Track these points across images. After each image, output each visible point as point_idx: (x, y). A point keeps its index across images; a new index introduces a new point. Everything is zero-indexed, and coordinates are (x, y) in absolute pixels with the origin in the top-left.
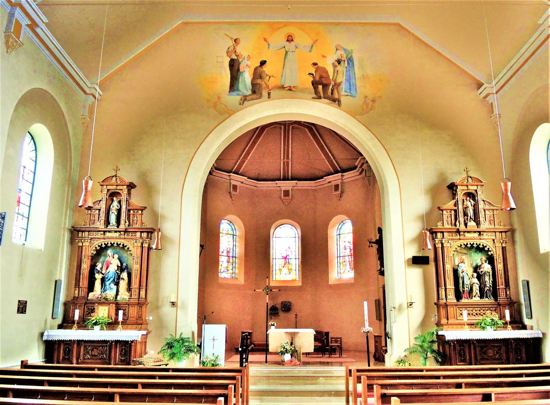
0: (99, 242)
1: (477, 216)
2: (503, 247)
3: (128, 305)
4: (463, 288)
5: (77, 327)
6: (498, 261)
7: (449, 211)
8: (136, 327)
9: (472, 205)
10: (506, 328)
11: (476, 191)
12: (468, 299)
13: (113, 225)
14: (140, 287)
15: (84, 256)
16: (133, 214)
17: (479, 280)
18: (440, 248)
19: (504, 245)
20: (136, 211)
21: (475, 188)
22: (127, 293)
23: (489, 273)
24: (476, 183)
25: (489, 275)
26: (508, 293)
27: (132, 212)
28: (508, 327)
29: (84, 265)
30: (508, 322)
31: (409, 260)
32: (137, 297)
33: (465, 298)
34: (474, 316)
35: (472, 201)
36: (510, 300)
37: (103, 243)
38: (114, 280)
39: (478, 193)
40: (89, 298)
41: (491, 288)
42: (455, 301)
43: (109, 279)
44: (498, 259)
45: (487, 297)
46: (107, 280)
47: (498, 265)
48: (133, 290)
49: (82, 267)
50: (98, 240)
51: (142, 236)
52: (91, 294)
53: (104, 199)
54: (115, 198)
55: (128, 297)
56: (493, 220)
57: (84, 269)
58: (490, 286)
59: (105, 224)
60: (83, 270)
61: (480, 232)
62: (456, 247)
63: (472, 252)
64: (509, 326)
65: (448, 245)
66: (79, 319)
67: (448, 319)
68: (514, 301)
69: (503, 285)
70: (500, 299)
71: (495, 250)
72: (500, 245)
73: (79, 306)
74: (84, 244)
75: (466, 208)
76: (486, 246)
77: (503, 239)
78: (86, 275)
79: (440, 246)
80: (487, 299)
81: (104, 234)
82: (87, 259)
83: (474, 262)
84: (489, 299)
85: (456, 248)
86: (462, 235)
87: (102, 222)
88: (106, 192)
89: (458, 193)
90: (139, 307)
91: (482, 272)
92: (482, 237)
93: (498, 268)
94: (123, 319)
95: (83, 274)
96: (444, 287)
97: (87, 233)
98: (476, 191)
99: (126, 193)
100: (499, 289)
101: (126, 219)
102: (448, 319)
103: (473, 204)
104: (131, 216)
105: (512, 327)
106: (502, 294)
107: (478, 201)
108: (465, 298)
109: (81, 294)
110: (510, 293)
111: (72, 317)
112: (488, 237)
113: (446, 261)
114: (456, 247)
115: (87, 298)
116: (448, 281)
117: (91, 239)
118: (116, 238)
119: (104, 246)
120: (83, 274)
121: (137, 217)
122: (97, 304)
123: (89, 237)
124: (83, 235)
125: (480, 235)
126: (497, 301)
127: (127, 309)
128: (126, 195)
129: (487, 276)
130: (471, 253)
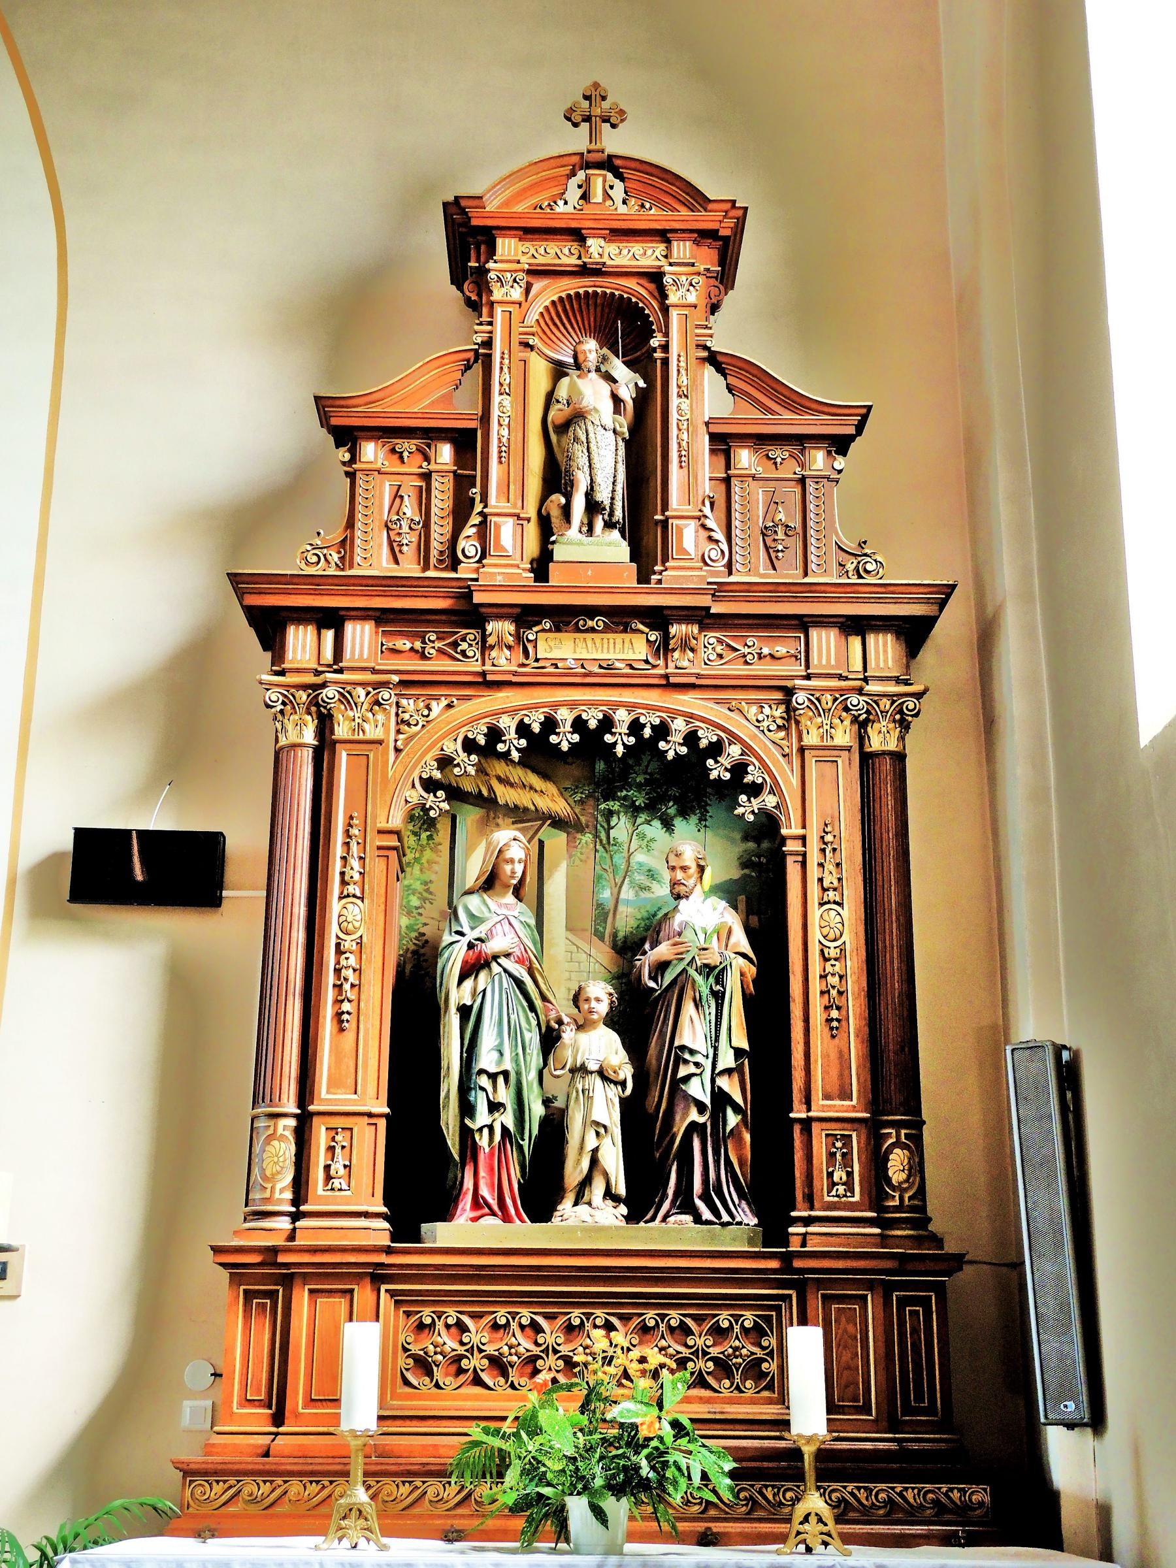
2: (867, 759)
4: (467, 1109)
6: (813, 872)
7: (407, 446)
9: (617, 400)
10: (779, 1513)
11: (655, 277)
12: (507, 1218)
17: (635, 1047)
18: (307, 755)
19: (881, 738)
21: (648, 255)
23: (719, 980)
24: (655, 216)
25: (719, 997)
26: (897, 1165)
28: (801, 1510)
30: (808, 1451)
31: (42, 870)
33: (478, 1203)
34: (477, 1381)
35: (619, 369)
36: (917, 1241)
39: (673, 298)
41: (733, 1120)
42: (379, 1232)
44: (814, 857)
45: (685, 1205)
47: (815, 913)
56: (796, 523)
57: (349, 943)
58: (720, 1099)
60: (339, 951)
61: (658, 618)
62: (453, 747)
63: (615, 805)
64: (814, 1502)
65: (372, 732)
67: (278, 1419)
68: (950, 1247)
69: (845, 1095)
70: (807, 1222)
71: (795, 781)
72: (844, 736)
75: (564, 428)
76: (716, 749)
77: (872, 687)
79: (309, 736)
80: (688, 1218)
83: (627, 893)
84: (698, 1219)
85: (445, 762)
86: (500, 643)
89: (498, 294)
91: (661, 967)
92: (682, 663)
93: (815, 935)
96: (290, 1106)
98: (655, 277)
100: (807, 1124)
102: (278, 1419)
103: (627, 394)
106: (839, 1175)
107: (666, 362)
108: (478, 1203)
110: (917, 1167)
112: (738, 669)
113: (337, 866)
114: (453, 747)
116: (336, 1050)
117: (403, 683)
125: (663, 648)
126: (784, 1240)
129: (698, 1004)
130: (610, 814)
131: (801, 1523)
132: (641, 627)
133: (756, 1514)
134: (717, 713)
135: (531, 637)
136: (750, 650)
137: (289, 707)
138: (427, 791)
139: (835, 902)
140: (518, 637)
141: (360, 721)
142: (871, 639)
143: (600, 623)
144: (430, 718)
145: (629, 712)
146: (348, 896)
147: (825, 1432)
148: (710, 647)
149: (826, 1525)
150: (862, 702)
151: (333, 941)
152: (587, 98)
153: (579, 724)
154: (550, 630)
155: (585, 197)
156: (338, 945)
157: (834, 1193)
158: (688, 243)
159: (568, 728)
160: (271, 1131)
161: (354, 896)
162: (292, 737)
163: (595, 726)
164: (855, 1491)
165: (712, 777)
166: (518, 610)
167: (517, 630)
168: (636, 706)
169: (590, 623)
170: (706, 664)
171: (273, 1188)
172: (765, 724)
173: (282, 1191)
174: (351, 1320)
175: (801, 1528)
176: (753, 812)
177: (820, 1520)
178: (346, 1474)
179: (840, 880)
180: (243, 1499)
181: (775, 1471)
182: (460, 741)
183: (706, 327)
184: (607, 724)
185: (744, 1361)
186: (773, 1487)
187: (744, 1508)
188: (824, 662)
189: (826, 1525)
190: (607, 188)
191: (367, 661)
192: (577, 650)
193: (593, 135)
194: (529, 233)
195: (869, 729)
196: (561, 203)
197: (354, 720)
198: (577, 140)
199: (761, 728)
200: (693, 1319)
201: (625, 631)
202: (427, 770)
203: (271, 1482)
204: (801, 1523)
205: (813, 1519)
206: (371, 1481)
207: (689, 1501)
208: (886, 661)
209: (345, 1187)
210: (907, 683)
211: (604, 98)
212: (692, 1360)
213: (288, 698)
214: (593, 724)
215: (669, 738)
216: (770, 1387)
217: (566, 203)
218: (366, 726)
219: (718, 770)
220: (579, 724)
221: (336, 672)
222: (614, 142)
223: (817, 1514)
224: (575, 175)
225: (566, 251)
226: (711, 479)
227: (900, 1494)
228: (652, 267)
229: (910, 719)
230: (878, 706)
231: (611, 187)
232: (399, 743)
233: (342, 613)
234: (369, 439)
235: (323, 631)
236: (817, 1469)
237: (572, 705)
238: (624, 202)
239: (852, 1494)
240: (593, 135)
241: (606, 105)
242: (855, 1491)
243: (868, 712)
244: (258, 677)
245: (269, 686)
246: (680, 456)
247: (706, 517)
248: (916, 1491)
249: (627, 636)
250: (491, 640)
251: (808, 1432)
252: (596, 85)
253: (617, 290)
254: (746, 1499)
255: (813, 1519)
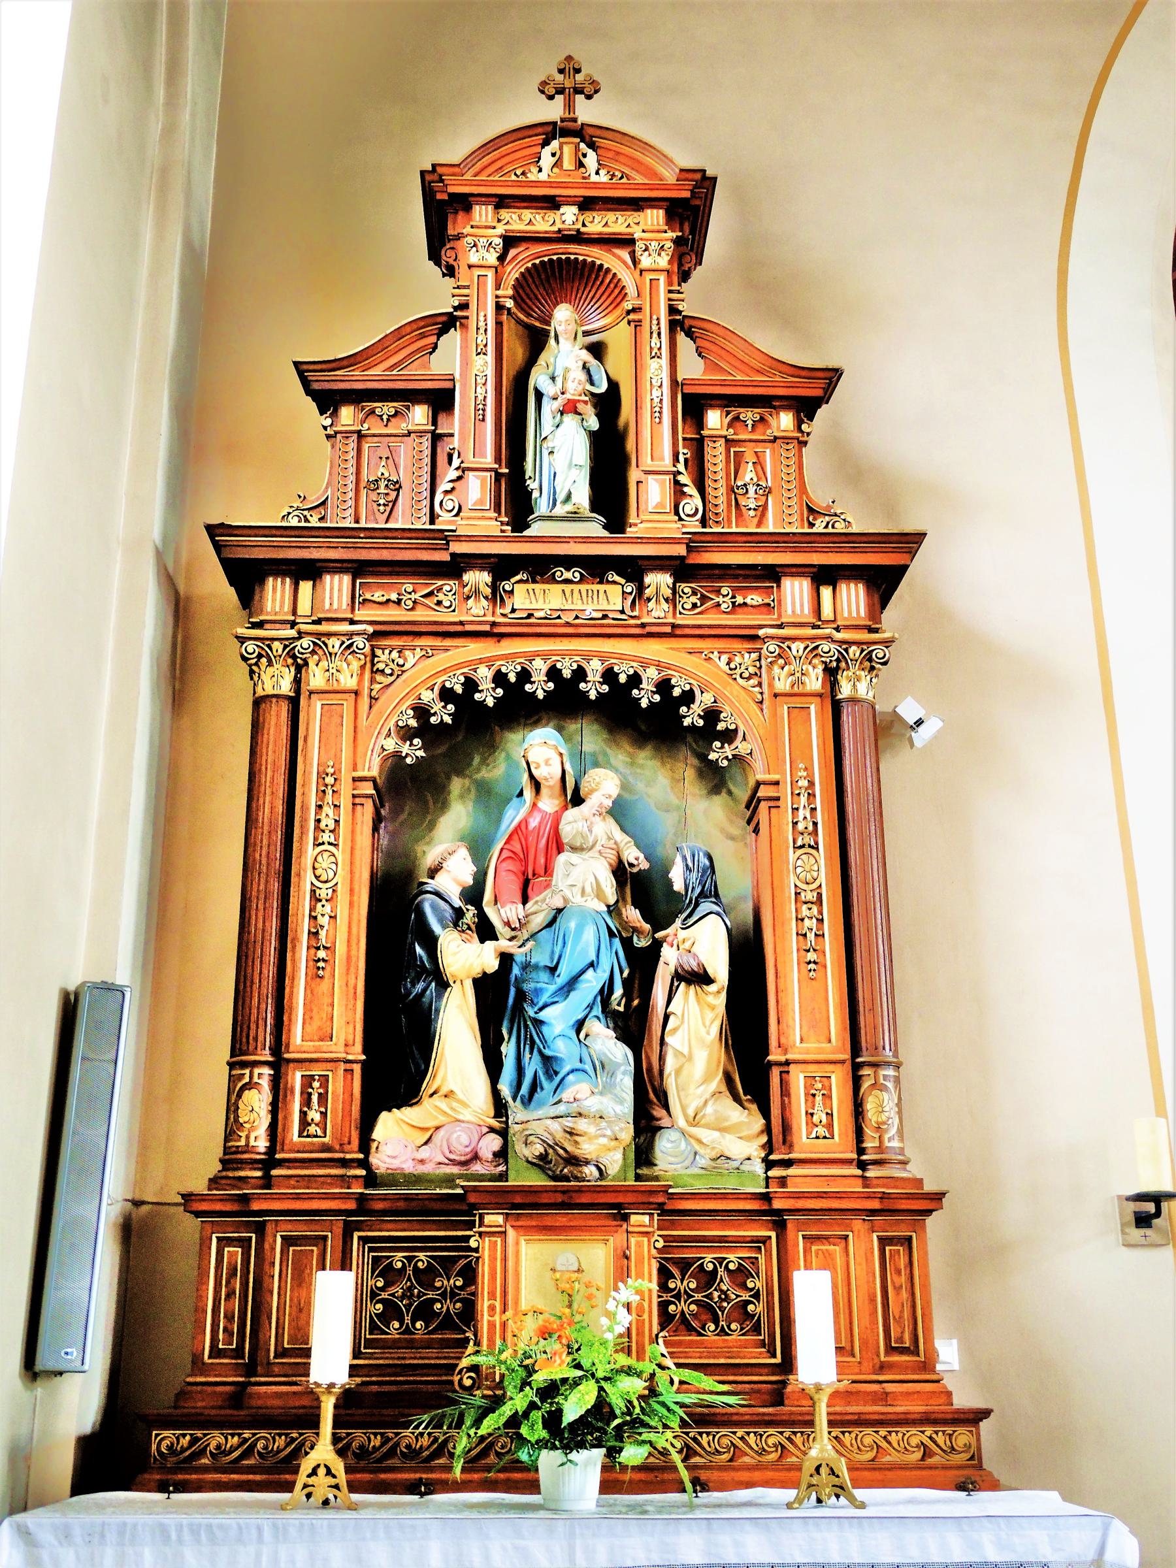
0: (441, 660)
1: (317, 1227)
3: (780, 1226)
5: (339, 1466)
8: (927, 1453)
13: (574, 517)
14: (856, 1050)
15: (322, 775)
16: (729, 442)
20: (749, 415)
22: (735, 1114)
27: (714, 419)
29: (325, 862)
32: (841, 1144)
37: (484, 675)
38: (605, 994)
40: (381, 1161)
43: (571, 985)
46: (548, 987)
48: (798, 1079)
49: (309, 877)
50: (438, 642)
51: (827, 612)
52: (388, 1125)
53: (483, 316)
54: (563, 316)
55: (754, 1149)
57: (323, 893)
59: (497, 509)
60: (315, 899)
66: (841, 1368)
73: (288, 1241)
74: (316, 678)
78: (341, 949)
81: (496, 596)
82: (345, 801)
87: (477, 489)
88: (492, 258)
90: (884, 1242)
94: (354, 1370)
95: (314, 935)
97: (337, 587)
99: (663, 261)
101: (681, 467)
104: (715, 455)
105: (541, 1388)
109: (304, 1123)
111: (215, 1352)
115: (365, 1164)
117: (377, 635)
118: (601, 627)
119: (488, 695)
120: (314, 935)
121: (759, 464)
122: (494, 1219)
123: (360, 614)
124: (304, 607)
127: (768, 1263)
128: (662, 278)
131: (309, 1476)
132: (617, 578)
133: (930, 1461)
134: (692, 663)
135: (507, 588)
136: (409, 596)
137: (264, 660)
138: (404, 739)
139: (330, 844)
140: (494, 587)
141: (334, 671)
142: (843, 587)
143: (577, 575)
144: (403, 669)
145: (545, 660)
146: (802, 846)
147: (834, 1378)
148: (685, 596)
149: (334, 1476)
150: (832, 649)
151: (308, 888)
152: (561, 71)
153: (553, 673)
154: (526, 582)
155: (558, 164)
156: (313, 892)
157: (305, 1134)
158: (490, 207)
159: (598, 678)
160: (247, 1079)
161: (810, 846)
162: (267, 686)
163: (569, 676)
164: (841, 1436)
165: (685, 724)
166: (815, 570)
167: (674, 584)
168: (612, 655)
169: (568, 575)
170: (454, 611)
171: (248, 1137)
172: (738, 671)
173: (890, 1140)
174: (324, 1269)
175: (310, 1481)
176: (727, 758)
177: (329, 1472)
178: (811, 1423)
179: (337, 822)
180: (496, 1450)
181: (282, 1418)
182: (437, 689)
183: (679, 292)
184: (580, 674)
185: (715, 1303)
186: (708, 1434)
187: (726, 1455)
188: (335, 606)
189: (334, 1476)
190: (580, 154)
191: (286, 614)
192: (547, 601)
193: (570, 105)
194: (501, 202)
195: (839, 677)
196: (534, 170)
197: (328, 670)
198: (554, 111)
199: (734, 676)
200: (674, 1263)
201: (601, 582)
202: (404, 718)
203: (239, 1435)
204: (309, 1476)
205: (322, 1471)
206: (836, 1432)
207: (764, 1450)
208: (282, 606)
209: (319, 1133)
210: (871, 630)
211: (578, 71)
212: (752, 1303)
213: (263, 649)
214: (567, 674)
215: (480, 688)
216: (757, 1329)
217: (540, 170)
218: (341, 677)
219: (692, 716)
220: (553, 673)
221: (314, 622)
222: (587, 112)
223: (326, 1466)
224: (548, 144)
225: (515, 217)
226: (684, 439)
227: (742, 1438)
228: (546, 232)
229: (878, 666)
230: (848, 654)
231: (585, 155)
232: (374, 693)
233: (319, 565)
234: (712, 407)
235: (301, 583)
236: (335, 1416)
237: (545, 655)
238: (597, 173)
239: (694, 1439)
240: (570, 105)
241: (579, 77)
242: (934, 1436)
243: (838, 660)
244: (234, 631)
245: (242, 640)
246: (484, 410)
247: (679, 473)
248: (900, 1435)
249: (602, 587)
250: (648, 592)
251: (324, 1381)
252: (569, 58)
253: (545, 256)
254: (775, 1445)
255: (322, 1471)
